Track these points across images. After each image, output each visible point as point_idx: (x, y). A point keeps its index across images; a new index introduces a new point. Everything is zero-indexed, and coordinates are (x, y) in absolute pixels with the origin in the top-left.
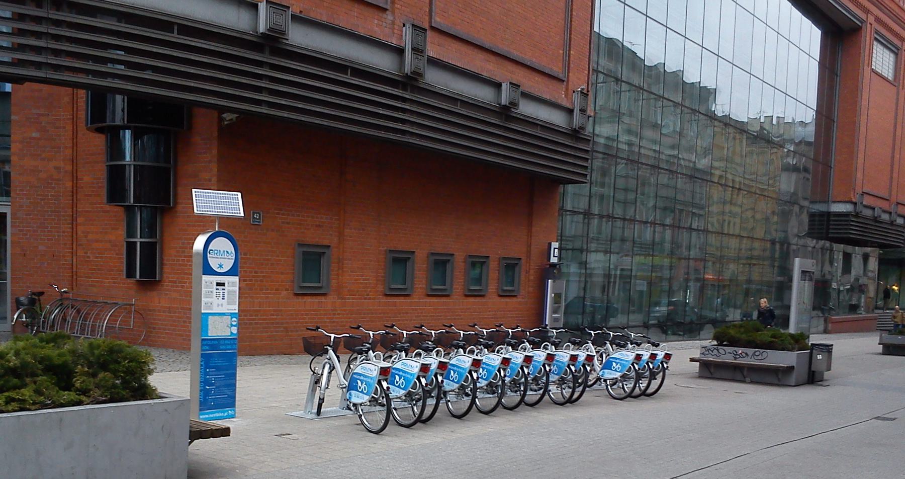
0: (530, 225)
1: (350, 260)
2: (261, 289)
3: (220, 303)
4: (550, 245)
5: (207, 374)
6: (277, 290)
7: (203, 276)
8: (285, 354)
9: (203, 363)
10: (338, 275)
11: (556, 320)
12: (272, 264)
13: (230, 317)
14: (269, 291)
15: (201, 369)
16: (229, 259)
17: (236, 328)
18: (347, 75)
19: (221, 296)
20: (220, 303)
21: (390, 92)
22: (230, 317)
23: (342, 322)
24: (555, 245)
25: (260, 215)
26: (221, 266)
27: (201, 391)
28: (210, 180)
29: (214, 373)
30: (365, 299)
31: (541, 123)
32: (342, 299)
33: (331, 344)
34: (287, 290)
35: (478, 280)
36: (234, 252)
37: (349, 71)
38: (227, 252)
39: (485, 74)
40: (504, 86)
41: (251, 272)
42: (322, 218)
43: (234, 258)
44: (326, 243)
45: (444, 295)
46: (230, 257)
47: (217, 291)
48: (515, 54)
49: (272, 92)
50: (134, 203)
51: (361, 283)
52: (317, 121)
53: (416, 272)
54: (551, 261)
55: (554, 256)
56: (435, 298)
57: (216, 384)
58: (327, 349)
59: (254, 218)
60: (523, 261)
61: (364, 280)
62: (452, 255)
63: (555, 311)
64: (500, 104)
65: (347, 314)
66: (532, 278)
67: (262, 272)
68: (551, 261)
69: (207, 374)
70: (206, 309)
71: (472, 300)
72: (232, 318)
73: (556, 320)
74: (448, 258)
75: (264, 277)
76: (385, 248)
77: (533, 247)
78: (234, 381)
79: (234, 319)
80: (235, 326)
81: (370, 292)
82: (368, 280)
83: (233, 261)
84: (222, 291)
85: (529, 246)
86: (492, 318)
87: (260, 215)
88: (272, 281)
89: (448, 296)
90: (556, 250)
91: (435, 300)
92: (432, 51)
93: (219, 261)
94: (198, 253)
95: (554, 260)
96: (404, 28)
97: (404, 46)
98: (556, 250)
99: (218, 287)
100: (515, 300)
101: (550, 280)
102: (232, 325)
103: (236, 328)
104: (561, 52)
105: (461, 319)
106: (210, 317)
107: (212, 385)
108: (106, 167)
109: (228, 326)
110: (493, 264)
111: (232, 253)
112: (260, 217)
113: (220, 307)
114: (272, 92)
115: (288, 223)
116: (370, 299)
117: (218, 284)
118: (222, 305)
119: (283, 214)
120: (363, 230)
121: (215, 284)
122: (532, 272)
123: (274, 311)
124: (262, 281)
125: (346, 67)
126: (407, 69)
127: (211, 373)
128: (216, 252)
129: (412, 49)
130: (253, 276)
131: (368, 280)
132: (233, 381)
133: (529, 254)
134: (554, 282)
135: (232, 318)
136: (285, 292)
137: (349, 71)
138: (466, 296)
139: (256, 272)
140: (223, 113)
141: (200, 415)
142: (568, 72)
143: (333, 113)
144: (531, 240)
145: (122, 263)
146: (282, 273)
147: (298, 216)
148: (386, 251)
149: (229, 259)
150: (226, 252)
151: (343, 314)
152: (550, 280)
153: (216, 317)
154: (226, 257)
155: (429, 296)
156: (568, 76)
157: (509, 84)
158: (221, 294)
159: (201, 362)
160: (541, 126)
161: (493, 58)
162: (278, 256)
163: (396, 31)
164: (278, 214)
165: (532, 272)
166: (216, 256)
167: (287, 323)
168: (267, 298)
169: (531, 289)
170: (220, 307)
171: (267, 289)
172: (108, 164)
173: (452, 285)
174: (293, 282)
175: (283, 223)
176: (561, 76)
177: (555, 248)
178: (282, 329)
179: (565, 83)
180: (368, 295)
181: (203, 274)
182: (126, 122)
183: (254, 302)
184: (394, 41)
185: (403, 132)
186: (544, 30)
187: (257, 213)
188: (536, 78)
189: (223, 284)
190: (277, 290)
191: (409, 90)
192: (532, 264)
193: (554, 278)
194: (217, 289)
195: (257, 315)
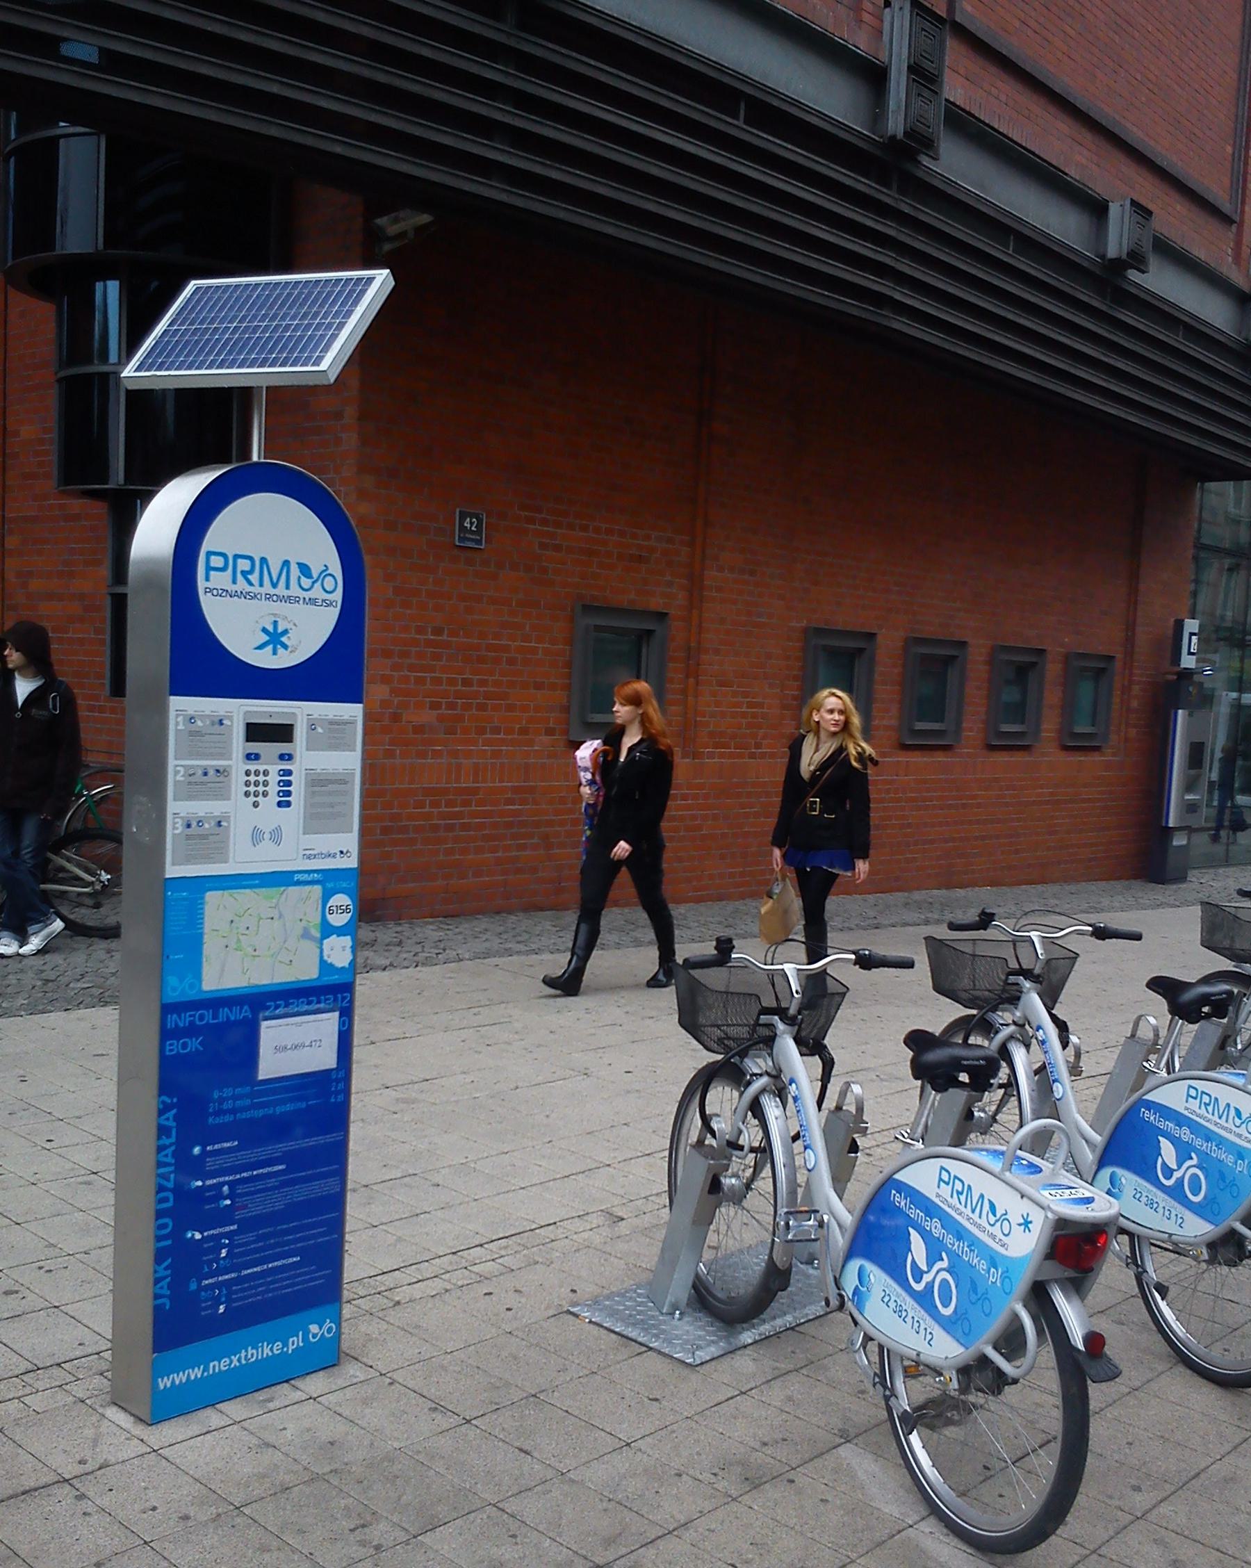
0: (1134, 577)
1: (717, 651)
2: (481, 731)
3: (267, 828)
4: (1179, 625)
5: (186, 1165)
6: (524, 731)
7: (172, 698)
8: (542, 909)
9: (170, 1120)
10: (684, 692)
11: (1192, 808)
12: (511, 661)
13: (318, 889)
14: (502, 736)
15: (160, 1149)
16: (313, 601)
17: (347, 941)
18: (736, 117)
19: (273, 789)
20: (267, 828)
21: (848, 182)
22: (318, 889)
23: (694, 817)
24: (1191, 625)
25: (480, 521)
26: (275, 638)
27: (159, 1257)
28: (339, 415)
29: (227, 1161)
30: (752, 756)
31: (1186, 319)
32: (696, 755)
33: (792, 1011)
34: (550, 732)
35: (1018, 711)
36: (336, 568)
37: (743, 106)
38: (305, 570)
39: (1073, 173)
40: (1114, 209)
41: (451, 682)
42: (648, 538)
43: (338, 596)
44: (656, 603)
45: (941, 746)
46: (317, 592)
47: (253, 767)
48: (1135, 133)
49: (522, 140)
50: (125, 484)
51: (744, 715)
52: (650, 240)
53: (877, 687)
54: (1183, 665)
55: (1190, 653)
56: (918, 753)
57: (238, 1215)
58: (771, 1026)
59: (461, 525)
60: (1118, 664)
61: (750, 705)
62: (963, 644)
63: (1189, 786)
64: (1103, 257)
65: (706, 797)
66: (1135, 704)
67: (483, 683)
68: (1183, 665)
69: (194, 1167)
70: (189, 860)
71: (1002, 758)
72: (326, 897)
73: (1192, 808)
74: (954, 653)
75: (487, 696)
76: (804, 624)
77: (1139, 629)
78: (329, 1186)
79: (341, 900)
80: (340, 931)
81: (764, 738)
82: (761, 705)
83: (332, 615)
84: (274, 769)
85: (1130, 627)
86: (1048, 802)
87: (480, 521)
88: (510, 708)
89: (946, 748)
90: (1194, 639)
91: (917, 758)
92: (955, 90)
93: (261, 613)
94: (149, 580)
95: (1188, 662)
96: (887, 10)
97: (886, 60)
98: (1194, 639)
99: (256, 747)
100: (1096, 757)
101: (1180, 712)
102: (328, 930)
103: (347, 941)
104: (1229, 149)
105: (979, 806)
106: (212, 898)
107: (225, 1217)
108: (56, 386)
109: (306, 935)
110: (1053, 669)
111: (325, 572)
112: (479, 526)
113: (267, 844)
114: (522, 140)
115: (557, 548)
116: (763, 755)
117: (256, 732)
118: (276, 836)
119: (544, 522)
120: (752, 573)
121: (239, 732)
122: (1136, 689)
123: (516, 790)
124: (482, 707)
125: (737, 95)
126: (895, 124)
127: (211, 1164)
128: (244, 565)
129: (909, 67)
130: (458, 695)
131: (761, 705)
132: (329, 1186)
133: (1129, 641)
134: (1190, 715)
135: (326, 897)
136: (545, 738)
137: (743, 106)
138: (992, 748)
139: (466, 682)
140: (380, 216)
141: (157, 1373)
142: (1243, 203)
143: (696, 223)
144: (1136, 609)
145: (102, 642)
146: (539, 686)
147: (584, 528)
148: (805, 630)
149: (313, 601)
150: (295, 571)
151: (695, 797)
152: (1180, 712)
153: (246, 896)
154: (295, 591)
155: (905, 748)
156: (1243, 212)
157: (1128, 203)
158: (274, 778)
159: (161, 1113)
160: (1186, 325)
161: (1087, 137)
162: (526, 639)
163: (866, 17)
164: (531, 520)
165: (1136, 689)
166: (241, 584)
167: (549, 823)
168: (495, 755)
169: (1133, 732)
170: (267, 844)
171: (496, 730)
172: (62, 374)
173: (959, 723)
174: (566, 709)
175: (543, 546)
176: (1226, 208)
177: (1192, 634)
178: (535, 841)
179: (1234, 227)
180: (758, 746)
181: (174, 692)
182: (101, 246)
183: (459, 766)
184: (860, 42)
185: (880, 300)
186: (1197, 86)
187: (471, 515)
188: (1178, 207)
189: (282, 733)
190: (524, 731)
191: (895, 186)
192: (1136, 671)
193: (1192, 708)
194: (249, 757)
195: (466, 803)
